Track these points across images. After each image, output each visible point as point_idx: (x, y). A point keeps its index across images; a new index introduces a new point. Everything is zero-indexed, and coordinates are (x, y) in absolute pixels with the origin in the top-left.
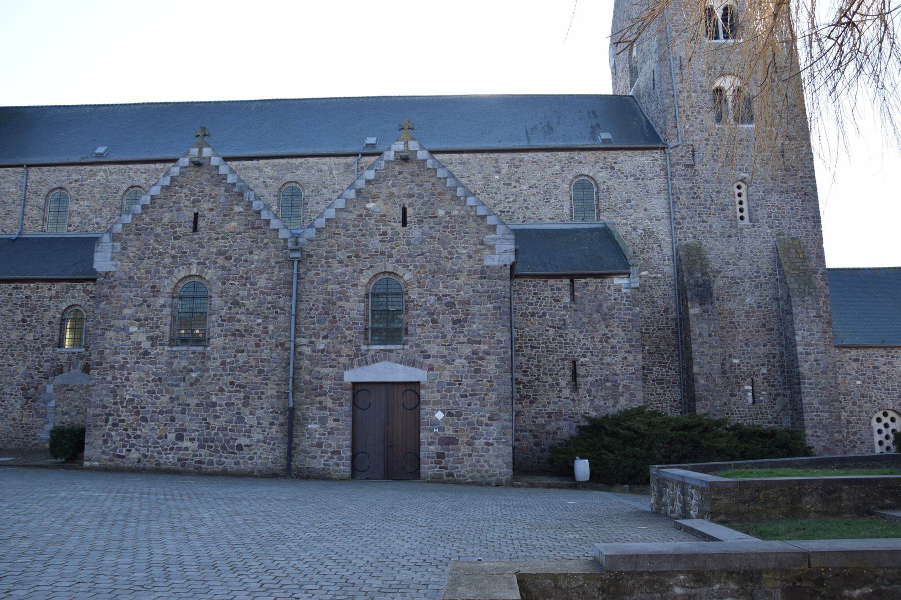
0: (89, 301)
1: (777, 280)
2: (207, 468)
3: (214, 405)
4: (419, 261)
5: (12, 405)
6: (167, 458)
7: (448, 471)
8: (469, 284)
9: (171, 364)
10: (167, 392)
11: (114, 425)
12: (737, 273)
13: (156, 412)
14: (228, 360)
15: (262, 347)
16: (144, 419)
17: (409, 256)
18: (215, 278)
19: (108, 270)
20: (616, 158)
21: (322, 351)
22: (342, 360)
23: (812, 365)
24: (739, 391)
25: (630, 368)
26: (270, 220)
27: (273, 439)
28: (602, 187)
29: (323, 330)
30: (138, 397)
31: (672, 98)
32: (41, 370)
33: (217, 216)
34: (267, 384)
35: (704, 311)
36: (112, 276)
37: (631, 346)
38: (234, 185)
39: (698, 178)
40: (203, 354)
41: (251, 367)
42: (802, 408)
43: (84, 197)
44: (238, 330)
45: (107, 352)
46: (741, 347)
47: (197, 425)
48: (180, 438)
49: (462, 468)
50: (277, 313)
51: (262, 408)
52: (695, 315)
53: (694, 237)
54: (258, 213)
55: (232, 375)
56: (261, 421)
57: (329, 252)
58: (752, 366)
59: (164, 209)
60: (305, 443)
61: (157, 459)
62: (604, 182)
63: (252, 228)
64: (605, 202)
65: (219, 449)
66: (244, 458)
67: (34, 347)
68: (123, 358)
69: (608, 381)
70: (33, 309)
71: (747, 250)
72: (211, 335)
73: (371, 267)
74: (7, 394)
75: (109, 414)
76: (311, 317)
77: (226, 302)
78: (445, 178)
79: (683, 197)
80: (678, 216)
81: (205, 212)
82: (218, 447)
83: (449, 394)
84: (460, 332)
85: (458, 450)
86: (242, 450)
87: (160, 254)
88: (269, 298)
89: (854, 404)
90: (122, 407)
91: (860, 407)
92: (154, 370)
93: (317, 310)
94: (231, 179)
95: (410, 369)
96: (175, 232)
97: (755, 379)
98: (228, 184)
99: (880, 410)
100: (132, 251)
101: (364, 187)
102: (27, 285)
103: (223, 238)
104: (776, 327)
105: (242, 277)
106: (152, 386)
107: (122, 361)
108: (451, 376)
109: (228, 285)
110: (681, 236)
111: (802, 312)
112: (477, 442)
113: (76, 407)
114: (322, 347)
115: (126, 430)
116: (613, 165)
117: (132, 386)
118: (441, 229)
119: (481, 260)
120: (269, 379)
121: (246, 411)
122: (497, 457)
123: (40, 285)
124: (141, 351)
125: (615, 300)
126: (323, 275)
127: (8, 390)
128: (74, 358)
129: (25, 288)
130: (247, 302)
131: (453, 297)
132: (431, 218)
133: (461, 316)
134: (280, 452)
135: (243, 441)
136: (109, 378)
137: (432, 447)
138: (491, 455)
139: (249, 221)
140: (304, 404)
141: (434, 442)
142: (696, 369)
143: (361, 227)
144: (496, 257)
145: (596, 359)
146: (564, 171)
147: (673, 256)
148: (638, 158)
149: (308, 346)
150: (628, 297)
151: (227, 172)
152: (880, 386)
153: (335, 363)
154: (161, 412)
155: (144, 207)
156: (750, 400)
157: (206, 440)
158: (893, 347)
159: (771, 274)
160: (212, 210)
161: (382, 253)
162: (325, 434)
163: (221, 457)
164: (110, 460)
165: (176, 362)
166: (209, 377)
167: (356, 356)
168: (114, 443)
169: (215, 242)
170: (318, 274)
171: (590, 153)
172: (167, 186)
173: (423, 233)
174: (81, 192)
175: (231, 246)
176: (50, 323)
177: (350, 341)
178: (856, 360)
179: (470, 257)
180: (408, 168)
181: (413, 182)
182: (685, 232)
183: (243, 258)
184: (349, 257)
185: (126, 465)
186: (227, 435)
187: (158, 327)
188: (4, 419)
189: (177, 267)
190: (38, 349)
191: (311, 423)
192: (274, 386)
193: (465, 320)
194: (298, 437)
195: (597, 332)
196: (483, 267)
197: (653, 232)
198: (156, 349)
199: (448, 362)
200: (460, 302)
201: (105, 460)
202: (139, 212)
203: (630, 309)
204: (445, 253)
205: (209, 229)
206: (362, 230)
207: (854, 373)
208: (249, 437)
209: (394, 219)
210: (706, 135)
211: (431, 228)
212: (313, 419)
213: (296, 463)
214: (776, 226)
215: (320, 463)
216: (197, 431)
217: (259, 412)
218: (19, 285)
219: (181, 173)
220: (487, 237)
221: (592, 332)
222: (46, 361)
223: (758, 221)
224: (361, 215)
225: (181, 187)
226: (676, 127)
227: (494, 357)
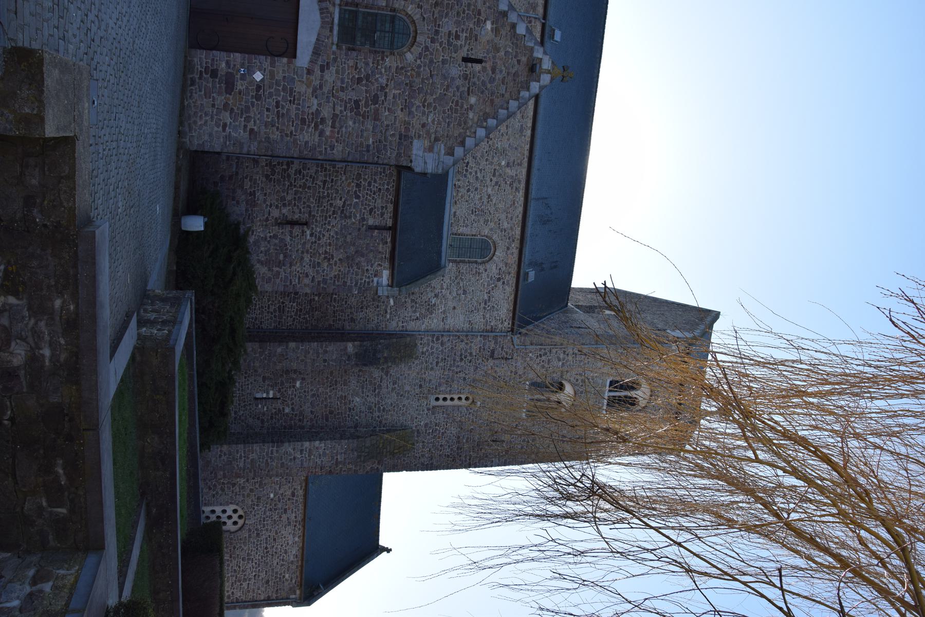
1: (375, 427)
4: (426, 72)
7: (197, 80)
8: (395, 121)
12: (384, 390)
17: (431, 61)
20: (508, 284)
23: (291, 454)
24: (268, 385)
25: (297, 281)
28: (482, 268)
46: (312, 390)
53: (423, 353)
58: (292, 399)
62: (486, 270)
64: (466, 269)
69: (285, 257)
71: (406, 402)
73: (424, 18)
78: (507, 109)
79: (463, 345)
80: (445, 339)
84: (346, 107)
85: (220, 94)
95: (311, 49)
97: (279, 401)
99: (245, 512)
101: (509, 21)
111: (342, 448)
112: (228, 114)
116: (502, 281)
118: (456, 99)
122: (210, 135)
125: (367, 270)
131: (383, 104)
132: (469, 88)
137: (224, 65)
141: (229, 68)
142: (292, 345)
143: (467, 12)
144: (421, 153)
145: (308, 246)
146: (502, 231)
148: (506, 305)
150: (369, 283)
152: (268, 514)
156: (258, 395)
158: (304, 527)
159: (381, 422)
161: (437, 32)
171: (517, 259)
173: (453, 79)
178: (293, 495)
179: (424, 125)
181: (508, 74)
193: (358, 114)
196: (412, 138)
199: (315, 91)
200: (378, 110)
206: (464, 13)
207: (281, 492)
211: (458, 88)
214: (426, 430)
220: (442, 145)
221: (336, 245)
223: (433, 413)
224: (479, 14)
226: (532, 344)
227: (317, 140)
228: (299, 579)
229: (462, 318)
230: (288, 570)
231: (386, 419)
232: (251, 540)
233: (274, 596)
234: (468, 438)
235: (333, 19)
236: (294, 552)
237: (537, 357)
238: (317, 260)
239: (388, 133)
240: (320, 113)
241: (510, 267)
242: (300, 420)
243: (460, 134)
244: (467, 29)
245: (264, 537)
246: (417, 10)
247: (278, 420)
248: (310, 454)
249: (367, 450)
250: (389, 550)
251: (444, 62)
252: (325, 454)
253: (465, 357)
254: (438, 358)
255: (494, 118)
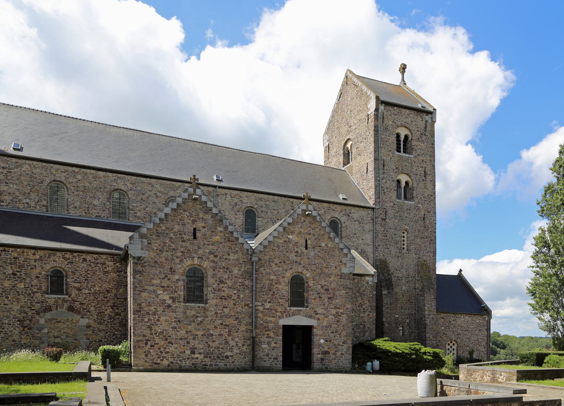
0: (67, 264)
1: (416, 280)
2: (209, 368)
3: (212, 335)
4: (314, 267)
5: (12, 331)
6: (186, 364)
7: (325, 366)
8: (335, 281)
9: (185, 313)
10: (184, 328)
11: (152, 346)
12: (400, 275)
13: (178, 339)
14: (219, 312)
15: (237, 306)
16: (171, 343)
17: (309, 264)
18: (209, 267)
19: (140, 256)
20: (350, 210)
21: (268, 309)
22: (278, 314)
23: (431, 320)
24: (397, 330)
25: (371, 319)
26: (238, 238)
27: (245, 352)
28: (344, 225)
29: (268, 298)
30: (166, 330)
31: (378, 182)
32: (33, 308)
33: (208, 232)
34: (240, 325)
35: (389, 293)
36: (143, 259)
37: (371, 309)
38: (216, 214)
39: (387, 226)
40: (204, 308)
41: (232, 316)
42: (425, 339)
43: (13, 182)
44: (224, 296)
45: (143, 305)
46: (399, 310)
47: (203, 346)
48: (193, 352)
49: (331, 365)
50: (244, 288)
51: (238, 337)
52: (385, 294)
53: (383, 256)
54: (232, 233)
55: (221, 320)
56: (238, 344)
57: (270, 259)
58: (403, 319)
59: (174, 223)
60: (260, 354)
61: (180, 364)
62: (345, 223)
63: (229, 241)
64: (345, 233)
65: (216, 358)
66: (229, 362)
67: (25, 293)
68: (154, 309)
69: (361, 325)
70: (21, 266)
71: (405, 264)
72: (208, 298)
73: (291, 268)
74: (5, 324)
75: (148, 340)
76: (262, 292)
77: (216, 281)
78: (325, 227)
79: (380, 235)
80: (377, 244)
81: (200, 228)
82: (215, 357)
83: (326, 331)
84: (331, 303)
85: (330, 357)
86: (228, 358)
87: (174, 249)
88: (240, 280)
89: (440, 337)
90: (156, 336)
91: (443, 339)
92: (175, 316)
93: (265, 289)
94: (215, 211)
95: (309, 319)
96: (183, 238)
97: (404, 325)
98: (213, 213)
99: (450, 340)
100: (155, 246)
101: (287, 226)
102: (13, 249)
103: (212, 245)
104: (414, 302)
105: (224, 267)
106: (174, 325)
107: (154, 310)
108: (327, 323)
109: (216, 272)
110: (377, 255)
111: (428, 296)
112: (337, 353)
113: (64, 333)
114: (268, 307)
115: (159, 349)
116: (349, 214)
117: (162, 325)
118: (323, 253)
119: (341, 270)
120: (241, 322)
121: (230, 338)
122: (346, 360)
123: (25, 250)
124: (166, 305)
125: (366, 287)
126: (268, 270)
127: (6, 321)
128: (60, 302)
129: (12, 251)
130: (228, 282)
131: (329, 287)
132: (319, 246)
133: (331, 296)
134: (248, 358)
135: (229, 354)
136: (146, 320)
137: (319, 356)
138: (343, 359)
139: (227, 237)
140: (260, 335)
141: (320, 353)
142: (384, 319)
143: (286, 248)
144: (347, 269)
145: (357, 315)
146: (326, 214)
147: (373, 264)
148: (361, 212)
149: (261, 306)
150: (371, 286)
151: (212, 206)
152: (450, 330)
153: (274, 315)
154: (181, 339)
155: (161, 219)
156: (401, 334)
157: (208, 354)
158: (457, 314)
159: (414, 277)
160: (204, 227)
161: (296, 262)
162: (270, 350)
163: (217, 362)
164: (150, 366)
165: (188, 311)
166: (208, 321)
167: (284, 312)
168: (152, 356)
169: (207, 246)
170: (265, 270)
171: (338, 206)
172: (175, 209)
173: (315, 254)
174: (9, 178)
175: (217, 250)
176: (37, 277)
177: (282, 305)
178: (443, 318)
179: (336, 268)
180: (308, 219)
181: (310, 227)
182: (379, 253)
183: (224, 257)
184: (280, 262)
185: (160, 368)
186: (220, 351)
187: (176, 292)
188: (5, 341)
189: (185, 258)
190: (29, 294)
191: (263, 345)
192: (244, 326)
193: (333, 297)
194: (256, 351)
195: (358, 302)
196: (341, 273)
197: (365, 251)
198: (175, 304)
199: (326, 317)
200: (331, 289)
201: (147, 366)
202: (158, 223)
203: (372, 292)
204: (325, 265)
205: (203, 238)
206: (286, 249)
208: (232, 351)
209: (302, 245)
210: (392, 204)
211: (319, 252)
212: (264, 342)
213: (257, 364)
214: (418, 254)
215: (268, 363)
216: (203, 349)
217: (237, 339)
218: (7, 249)
219: (183, 202)
220: (343, 259)
221: (355, 301)
222: (36, 303)
223: (411, 251)
224: (285, 241)
225: (184, 211)
226: (379, 198)
227: (345, 315)
228: (479, 316)
229: (367, 236)
230: (475, 321)
231: (413, 274)
232: (461, 337)
233: (486, 327)
234: (422, 233)
235: (296, 310)
236: (468, 318)
237: (385, 195)
238: (362, 310)
239: (340, 284)
240: (334, 314)
241: (343, 209)
242: (412, 315)
243: (338, 250)
244: (293, 247)
245: (460, 332)
246: (288, 271)
247: (412, 325)
248: (430, 311)
249: (429, 284)
250: (461, 271)
251: (308, 259)
252: (431, 304)
253: (385, 234)
254: (385, 248)
255: (330, 234)
